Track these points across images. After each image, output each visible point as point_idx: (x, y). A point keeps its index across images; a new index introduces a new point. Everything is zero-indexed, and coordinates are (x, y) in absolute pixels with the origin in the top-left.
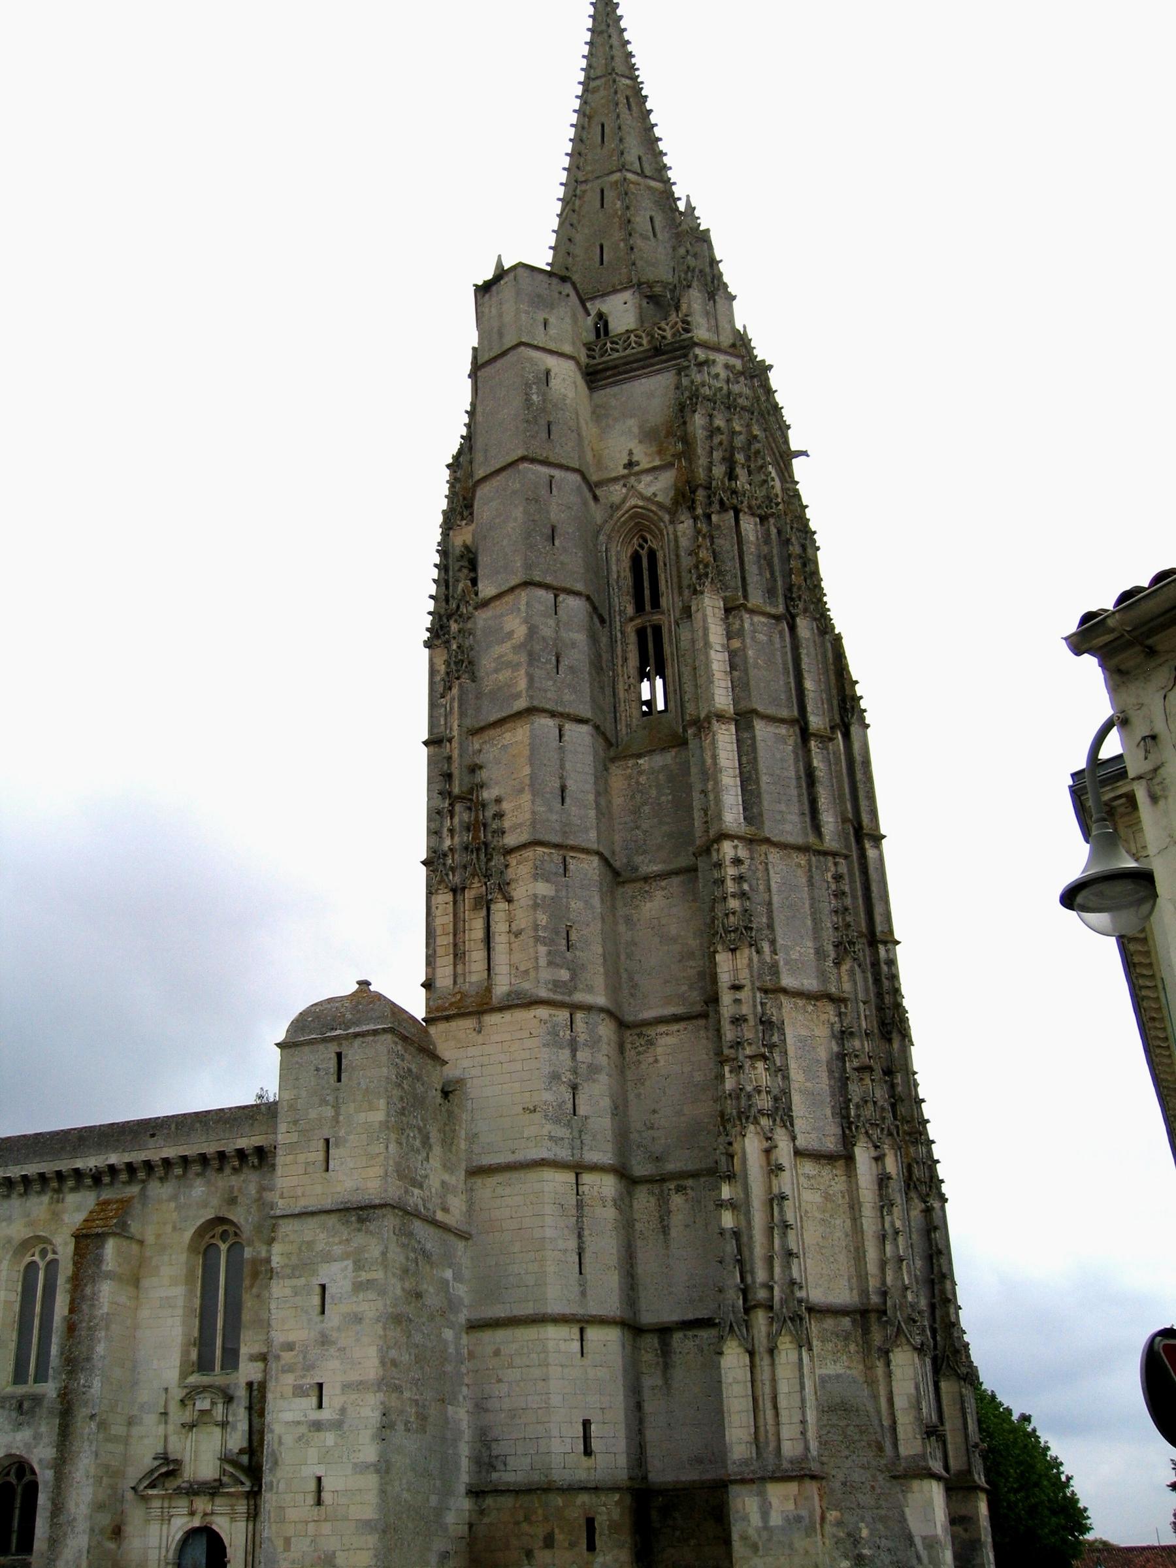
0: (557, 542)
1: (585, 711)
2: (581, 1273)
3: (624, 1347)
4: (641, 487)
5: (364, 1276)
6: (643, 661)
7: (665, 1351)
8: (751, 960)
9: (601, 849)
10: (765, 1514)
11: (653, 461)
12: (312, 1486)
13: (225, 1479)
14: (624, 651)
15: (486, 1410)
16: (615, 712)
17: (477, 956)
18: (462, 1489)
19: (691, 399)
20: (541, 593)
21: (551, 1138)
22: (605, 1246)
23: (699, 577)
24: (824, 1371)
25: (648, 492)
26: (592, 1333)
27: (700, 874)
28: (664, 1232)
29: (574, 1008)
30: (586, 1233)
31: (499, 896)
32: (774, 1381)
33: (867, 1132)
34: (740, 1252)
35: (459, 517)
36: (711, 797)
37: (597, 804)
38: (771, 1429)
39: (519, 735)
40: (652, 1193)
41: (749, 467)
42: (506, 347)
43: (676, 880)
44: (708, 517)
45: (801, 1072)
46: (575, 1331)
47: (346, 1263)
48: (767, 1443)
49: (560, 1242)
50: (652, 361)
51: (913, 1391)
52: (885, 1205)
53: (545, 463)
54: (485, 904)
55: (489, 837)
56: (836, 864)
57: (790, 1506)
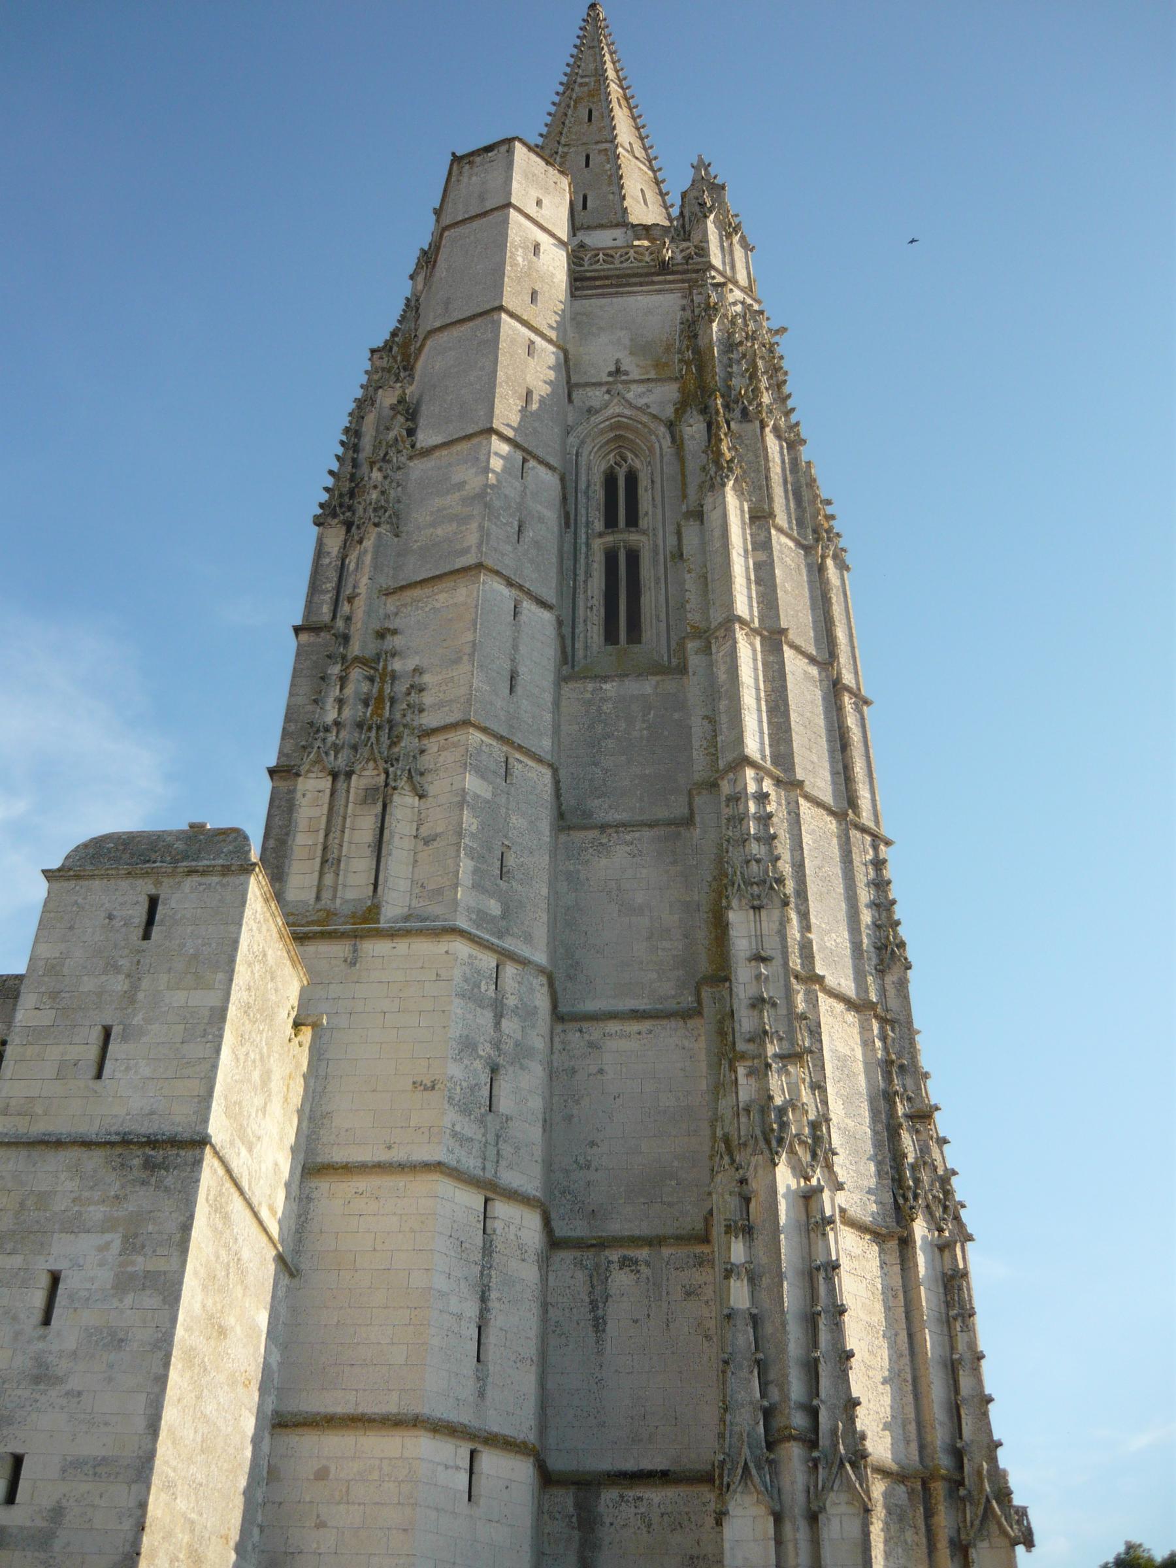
2: (478, 1360)
4: (630, 396)
5: (140, 1263)
21: (455, 1134)
22: (516, 1323)
25: (641, 402)
28: (596, 1326)
29: (506, 955)
30: (494, 1295)
33: (928, 1206)
35: (393, 378)
40: (578, 1264)
43: (647, 834)
47: (108, 1237)
49: (454, 1300)
50: (656, 279)
54: (381, 797)
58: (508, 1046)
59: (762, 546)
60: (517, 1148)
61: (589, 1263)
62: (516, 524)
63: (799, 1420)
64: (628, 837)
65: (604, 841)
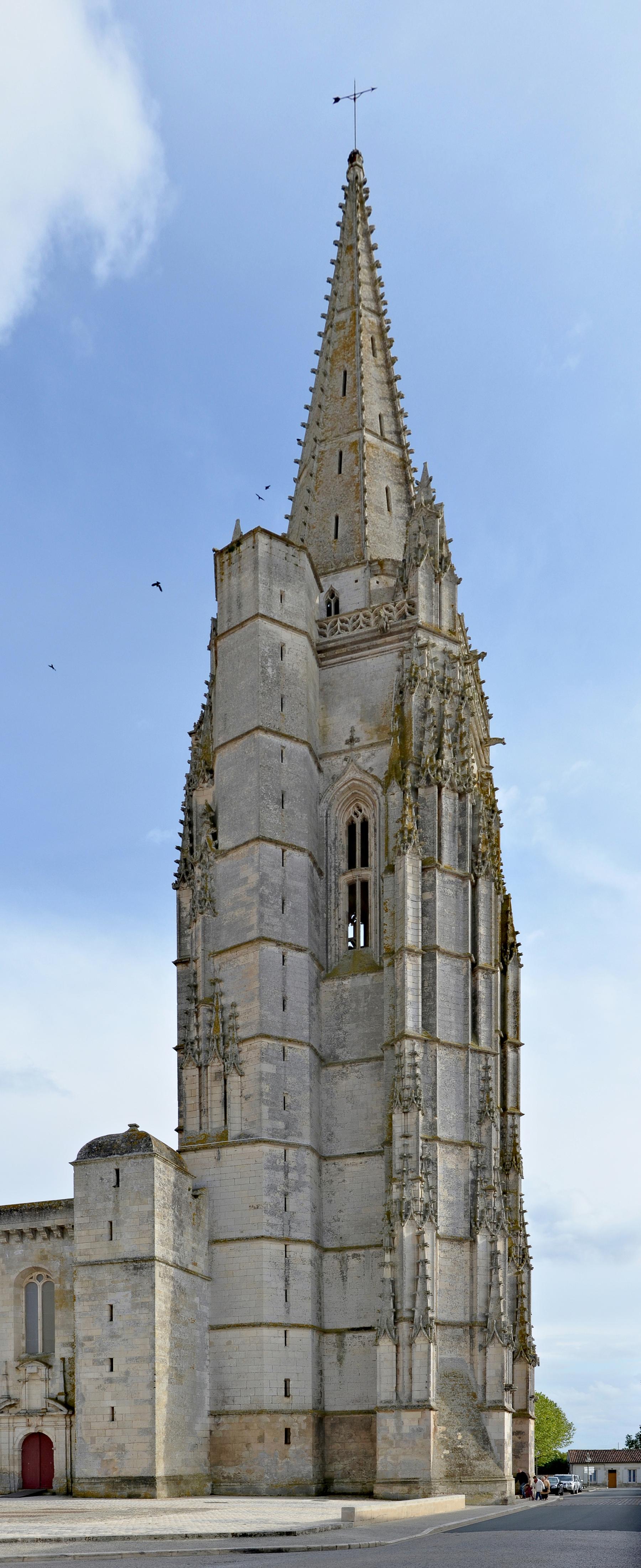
0: (285, 806)
1: (304, 942)
3: (313, 1340)
5: (139, 1300)
6: (352, 909)
7: (341, 1345)
8: (418, 1119)
9: (312, 1043)
10: (399, 1427)
11: (372, 738)
12: (109, 1411)
13: (49, 1408)
14: (337, 899)
15: (221, 1373)
16: (327, 945)
17: (217, 1111)
18: (206, 1413)
19: (410, 681)
20: (271, 847)
22: (302, 1287)
23: (403, 841)
24: (443, 1356)
25: (367, 766)
26: (292, 1333)
27: (384, 1062)
29: (289, 1145)
30: (291, 1279)
31: (234, 1072)
32: (411, 1360)
34: (394, 1291)
35: (201, 780)
36: (398, 1008)
37: (310, 1011)
38: (407, 1385)
39: (249, 957)
40: (335, 1257)
41: (455, 748)
42: (244, 618)
43: (366, 1065)
44: (415, 790)
45: (446, 1190)
46: (281, 1331)
48: (404, 1392)
51: (500, 1368)
52: (493, 1266)
53: (278, 733)
55: (227, 1031)
56: (486, 1060)
57: (415, 1424)
58: (292, 1184)
59: (427, 887)
60: (299, 1224)
61: (340, 1257)
62: (280, 900)
63: (407, 1315)
64: (356, 1068)
65: (345, 1071)
